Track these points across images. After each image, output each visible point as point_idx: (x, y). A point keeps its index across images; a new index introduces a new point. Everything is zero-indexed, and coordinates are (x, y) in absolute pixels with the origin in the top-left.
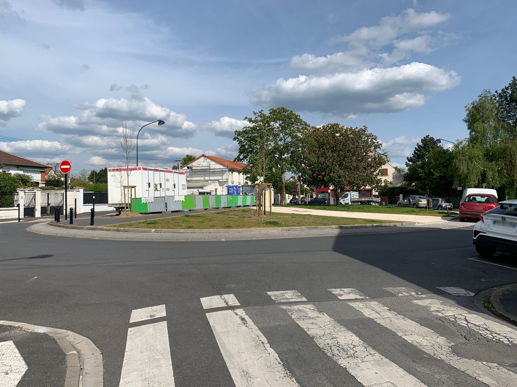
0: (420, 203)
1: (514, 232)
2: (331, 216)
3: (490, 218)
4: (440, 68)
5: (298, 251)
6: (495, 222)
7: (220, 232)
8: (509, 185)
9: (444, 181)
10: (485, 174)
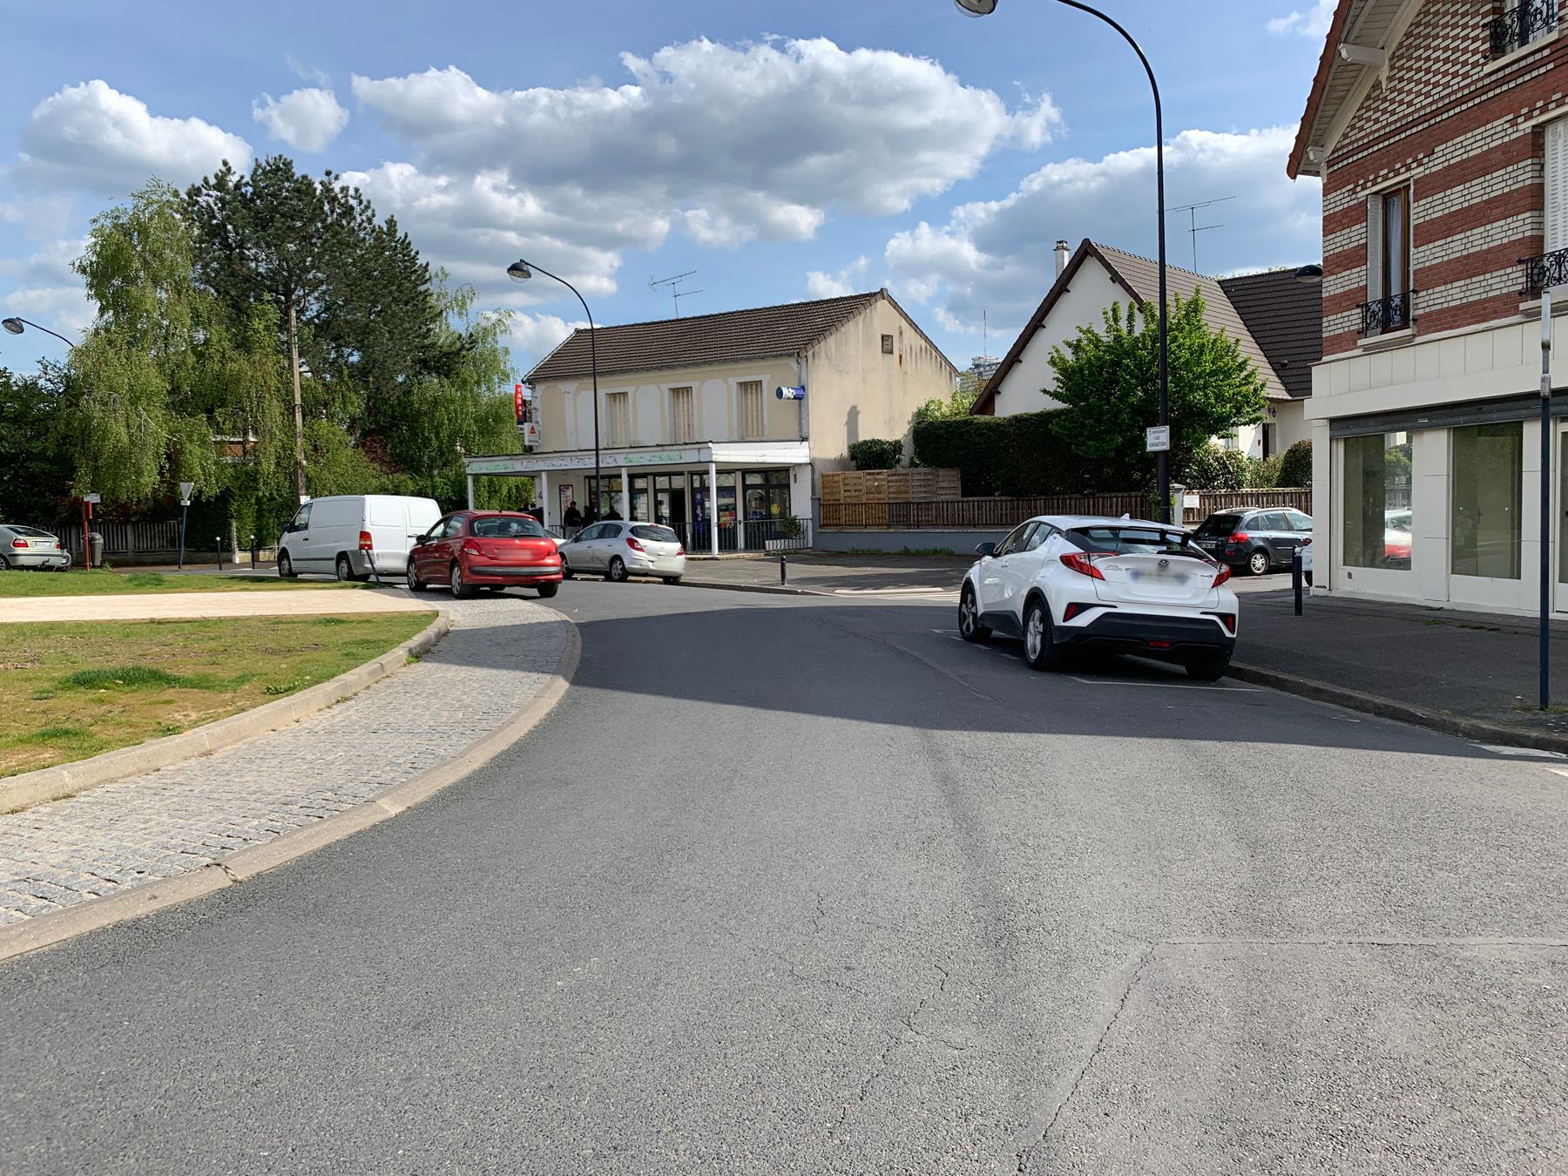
0: (19, 550)
1: (1189, 596)
2: (116, 622)
3: (1123, 566)
4: (492, 92)
5: (82, 798)
6: (1136, 575)
7: (111, 774)
8: (239, 488)
9: (12, 472)
10: (180, 452)
